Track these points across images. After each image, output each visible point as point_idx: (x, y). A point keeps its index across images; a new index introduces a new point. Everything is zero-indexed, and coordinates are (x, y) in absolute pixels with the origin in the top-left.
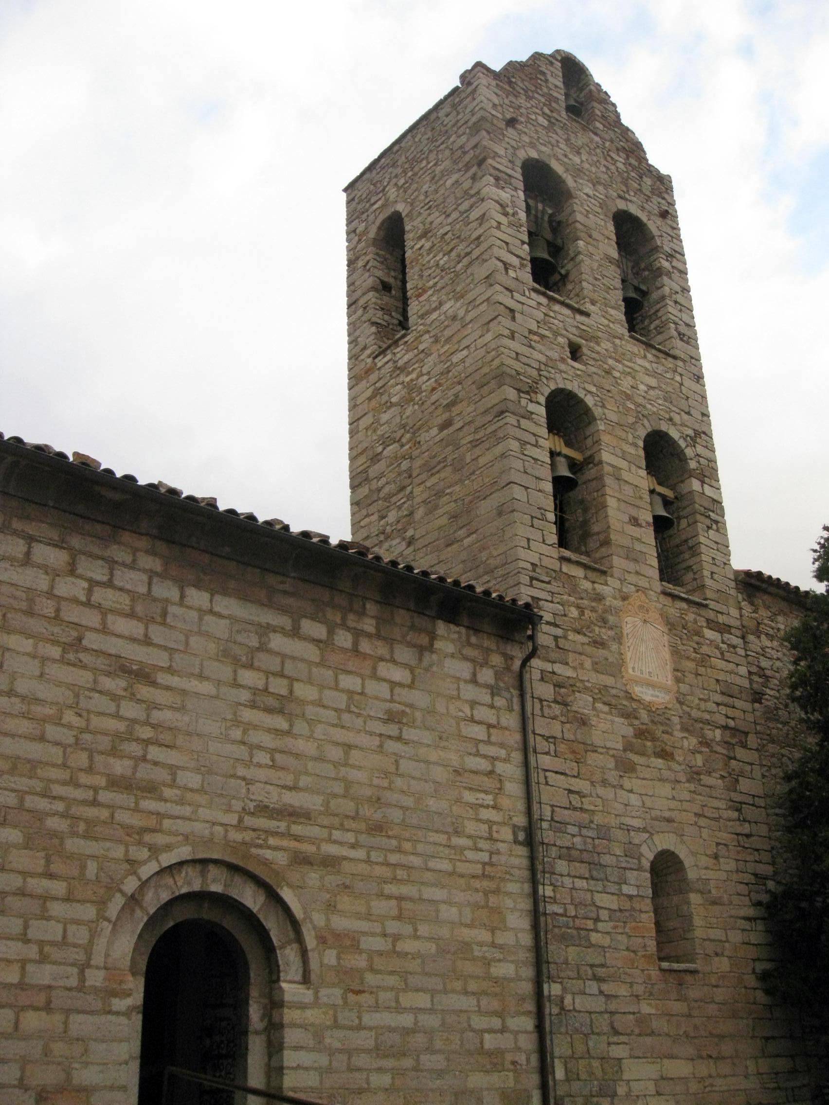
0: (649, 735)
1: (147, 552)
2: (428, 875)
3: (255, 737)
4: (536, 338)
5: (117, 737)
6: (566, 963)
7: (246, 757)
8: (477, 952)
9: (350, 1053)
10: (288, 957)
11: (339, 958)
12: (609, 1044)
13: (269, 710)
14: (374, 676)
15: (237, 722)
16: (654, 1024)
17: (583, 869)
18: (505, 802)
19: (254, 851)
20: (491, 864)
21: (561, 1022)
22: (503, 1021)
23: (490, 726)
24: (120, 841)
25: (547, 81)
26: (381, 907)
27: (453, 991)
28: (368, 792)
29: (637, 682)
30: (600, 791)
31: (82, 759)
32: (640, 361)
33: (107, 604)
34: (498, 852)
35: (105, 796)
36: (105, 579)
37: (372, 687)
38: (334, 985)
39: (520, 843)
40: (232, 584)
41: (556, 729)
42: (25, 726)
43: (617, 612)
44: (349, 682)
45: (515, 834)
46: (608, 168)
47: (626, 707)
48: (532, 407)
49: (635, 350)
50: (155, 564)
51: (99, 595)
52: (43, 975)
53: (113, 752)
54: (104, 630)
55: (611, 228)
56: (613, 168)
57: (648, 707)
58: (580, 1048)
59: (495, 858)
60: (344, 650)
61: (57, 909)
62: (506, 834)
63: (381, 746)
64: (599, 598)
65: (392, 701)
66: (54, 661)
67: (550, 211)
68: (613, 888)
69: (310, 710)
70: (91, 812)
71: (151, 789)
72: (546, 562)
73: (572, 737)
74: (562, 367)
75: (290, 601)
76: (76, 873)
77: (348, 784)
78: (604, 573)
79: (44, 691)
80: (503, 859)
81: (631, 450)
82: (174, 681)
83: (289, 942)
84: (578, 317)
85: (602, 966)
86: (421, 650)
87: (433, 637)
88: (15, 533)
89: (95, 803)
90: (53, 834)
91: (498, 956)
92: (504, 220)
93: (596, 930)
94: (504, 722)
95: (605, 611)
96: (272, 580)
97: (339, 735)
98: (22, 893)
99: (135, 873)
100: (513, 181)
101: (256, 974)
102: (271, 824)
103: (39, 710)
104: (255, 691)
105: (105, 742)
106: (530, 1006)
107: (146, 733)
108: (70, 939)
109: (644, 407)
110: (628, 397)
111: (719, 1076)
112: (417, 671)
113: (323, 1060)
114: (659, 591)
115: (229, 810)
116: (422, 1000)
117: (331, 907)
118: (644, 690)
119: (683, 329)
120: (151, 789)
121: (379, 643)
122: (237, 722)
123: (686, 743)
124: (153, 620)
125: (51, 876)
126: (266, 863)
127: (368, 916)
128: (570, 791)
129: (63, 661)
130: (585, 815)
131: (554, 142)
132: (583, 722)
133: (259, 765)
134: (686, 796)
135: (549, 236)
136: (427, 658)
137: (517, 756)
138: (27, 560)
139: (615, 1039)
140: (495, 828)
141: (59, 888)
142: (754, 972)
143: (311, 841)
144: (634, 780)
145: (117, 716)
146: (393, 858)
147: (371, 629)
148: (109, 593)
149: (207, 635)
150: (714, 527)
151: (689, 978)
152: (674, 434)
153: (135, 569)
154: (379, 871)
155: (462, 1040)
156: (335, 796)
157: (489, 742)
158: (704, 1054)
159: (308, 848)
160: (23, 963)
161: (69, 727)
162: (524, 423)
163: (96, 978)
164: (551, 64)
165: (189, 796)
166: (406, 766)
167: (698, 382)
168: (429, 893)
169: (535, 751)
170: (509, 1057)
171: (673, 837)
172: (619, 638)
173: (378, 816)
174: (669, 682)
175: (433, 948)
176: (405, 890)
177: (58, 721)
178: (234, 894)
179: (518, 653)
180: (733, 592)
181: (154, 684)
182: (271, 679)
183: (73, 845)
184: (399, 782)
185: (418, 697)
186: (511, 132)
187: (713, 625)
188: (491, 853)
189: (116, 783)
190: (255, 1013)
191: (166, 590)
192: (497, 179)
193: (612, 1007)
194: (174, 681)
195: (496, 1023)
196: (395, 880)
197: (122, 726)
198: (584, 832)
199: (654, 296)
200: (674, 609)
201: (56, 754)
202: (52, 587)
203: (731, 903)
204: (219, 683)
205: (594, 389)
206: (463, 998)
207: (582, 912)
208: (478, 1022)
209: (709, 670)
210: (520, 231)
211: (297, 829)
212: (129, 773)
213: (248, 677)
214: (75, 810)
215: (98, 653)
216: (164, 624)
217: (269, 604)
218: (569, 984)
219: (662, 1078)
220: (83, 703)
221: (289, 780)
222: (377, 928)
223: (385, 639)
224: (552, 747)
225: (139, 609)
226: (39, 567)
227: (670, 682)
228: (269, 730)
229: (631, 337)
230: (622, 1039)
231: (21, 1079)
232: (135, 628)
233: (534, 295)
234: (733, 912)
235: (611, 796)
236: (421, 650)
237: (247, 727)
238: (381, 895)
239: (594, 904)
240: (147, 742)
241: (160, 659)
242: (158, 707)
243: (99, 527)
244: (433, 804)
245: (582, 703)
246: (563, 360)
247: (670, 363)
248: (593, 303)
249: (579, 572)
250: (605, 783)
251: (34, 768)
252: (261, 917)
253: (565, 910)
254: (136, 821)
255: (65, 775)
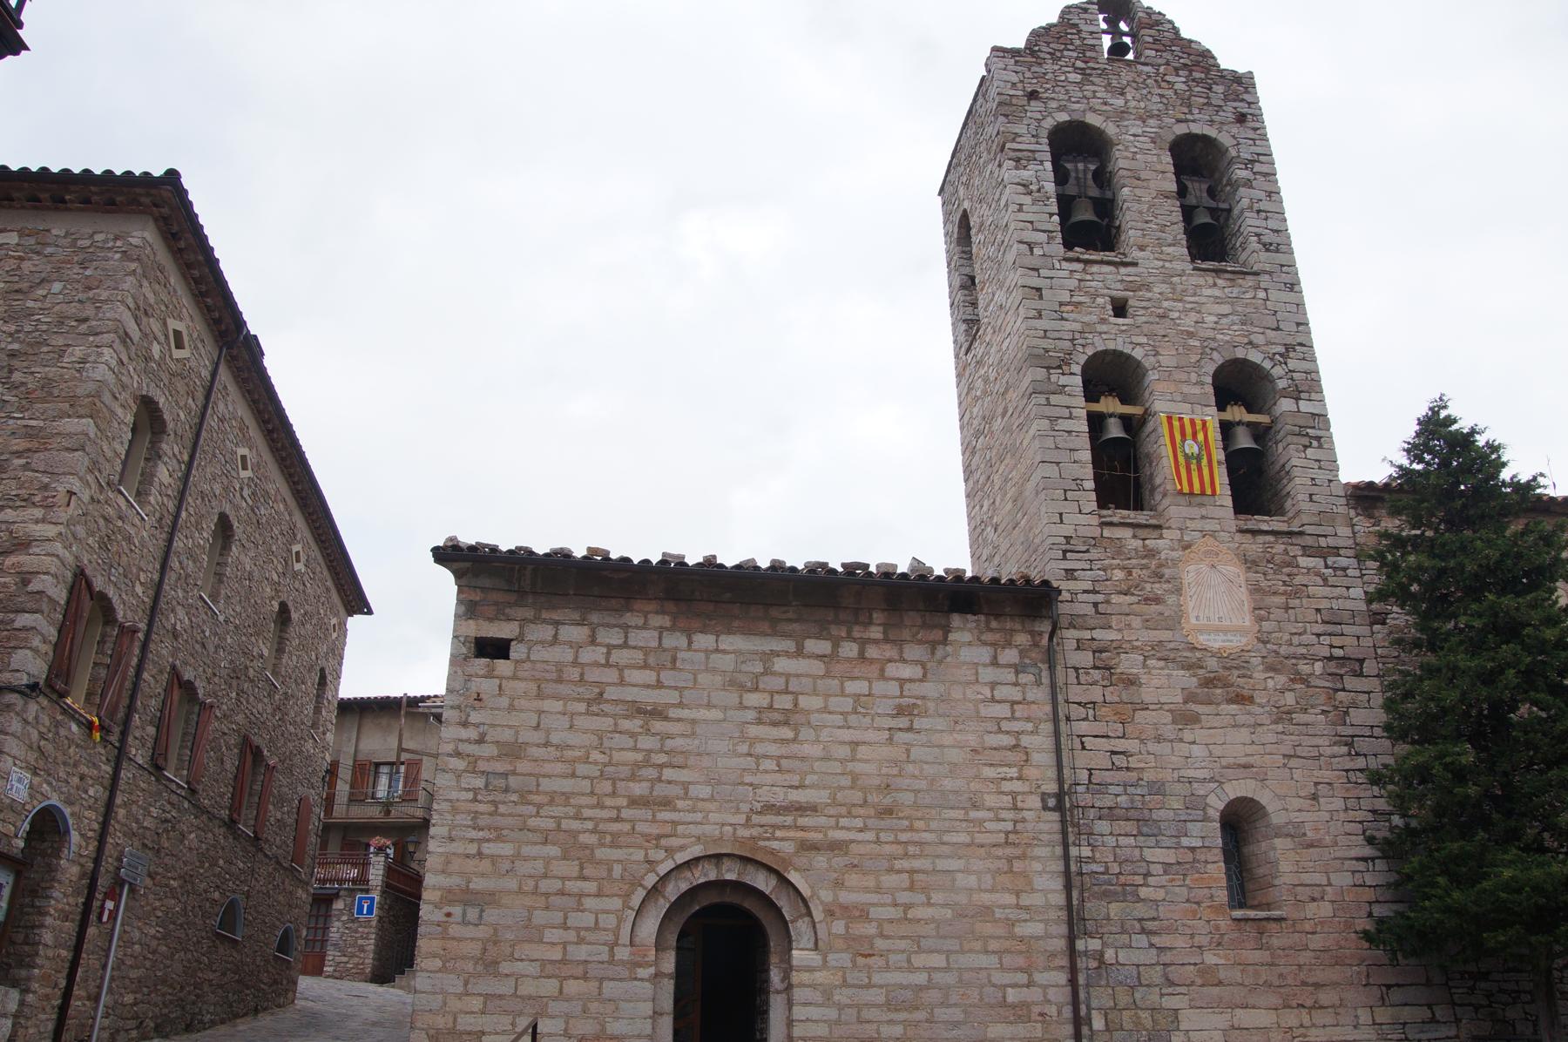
0: (1219, 682)
1: (657, 613)
2: (945, 848)
3: (759, 749)
4: (1069, 308)
5: (637, 765)
6: (1108, 919)
7: (754, 766)
8: (999, 914)
9: (859, 1008)
10: (800, 929)
11: (847, 928)
12: (1162, 995)
13: (775, 724)
14: (882, 676)
15: (743, 738)
16: (1222, 975)
17: (1130, 827)
18: (1032, 772)
19: (761, 843)
20: (1015, 832)
21: (1100, 975)
22: (1030, 975)
23: (1013, 703)
24: (641, 847)
25: (1080, 31)
26: (889, 880)
27: (971, 951)
28: (877, 781)
29: (1200, 631)
30: (1152, 747)
31: (607, 786)
32: (1209, 292)
33: (622, 662)
34: (1024, 820)
35: (625, 814)
36: (620, 642)
37: (879, 687)
38: (842, 951)
39: (1050, 809)
40: (736, 624)
41: (1096, 694)
42: (559, 768)
43: (1175, 563)
44: (852, 687)
45: (1043, 800)
46: (1162, 96)
47: (1189, 659)
48: (1063, 380)
49: (1201, 281)
50: (666, 621)
51: (616, 656)
52: (581, 953)
53: (633, 778)
54: (622, 682)
55: (1168, 158)
56: (1170, 92)
57: (1217, 654)
58: (1124, 999)
59: (1019, 826)
60: (849, 660)
61: (589, 903)
62: (1035, 802)
63: (891, 739)
64: (1151, 553)
65: (902, 696)
66: (581, 714)
67: (1092, 167)
68: (1167, 842)
69: (814, 718)
70: (615, 827)
71: (667, 803)
72: (1083, 531)
73: (1117, 699)
74: (1104, 328)
75: (796, 626)
76: (605, 874)
77: (855, 778)
78: (1159, 527)
79: (572, 738)
80: (1029, 826)
81: (1196, 390)
82: (685, 713)
83: (801, 916)
84: (1123, 270)
85: (1154, 919)
86: (933, 645)
87: (947, 630)
88: (544, 621)
89: (618, 819)
90: (586, 847)
91: (1026, 916)
92: (1027, 200)
93: (1146, 885)
94: (1030, 696)
95: (1160, 566)
96: (774, 612)
97: (847, 735)
98: (562, 893)
99: (654, 871)
100: (1037, 155)
101: (774, 943)
102: (779, 820)
103: (569, 754)
104: (760, 710)
105: (625, 771)
106: (1065, 962)
107: (662, 759)
108: (601, 925)
109: (1214, 339)
110: (1191, 335)
111: (1314, 1025)
112: (929, 665)
113: (833, 1014)
114: (1234, 529)
115: (738, 811)
116: (938, 960)
117: (838, 884)
118: (1212, 636)
119: (1268, 237)
120: (667, 803)
121: (888, 646)
122: (743, 738)
123: (1270, 683)
124: (663, 667)
125: (585, 879)
126: (773, 852)
127: (878, 889)
128: (1113, 753)
129: (588, 713)
130: (1134, 774)
131: (1089, 94)
132: (1131, 682)
133: (766, 772)
134: (1271, 738)
135: (1094, 192)
136: (940, 651)
137: (1047, 727)
138: (555, 641)
139: (1170, 990)
140: (1019, 798)
141: (591, 887)
142: (1370, 915)
143: (816, 829)
144: (1197, 731)
145: (635, 749)
146: (904, 837)
147: (880, 636)
148: (625, 653)
149: (714, 671)
150: (1315, 443)
151: (1273, 926)
152: (1255, 357)
153: (647, 630)
154: (888, 849)
155: (981, 994)
156: (841, 788)
157: (1013, 718)
158: (1294, 1004)
159: (815, 836)
160: (565, 945)
161: (596, 763)
162: (1054, 399)
163: (623, 953)
164: (1086, 11)
165: (700, 805)
166: (916, 753)
167: (1292, 290)
168: (942, 864)
169: (1068, 719)
170: (1036, 1009)
171: (1252, 784)
172: (1178, 591)
173: (888, 801)
174: (1247, 623)
175: (949, 913)
176: (917, 864)
177: (586, 760)
178: (747, 880)
179: (1045, 627)
180: (1342, 510)
181: (666, 718)
182: (776, 697)
183: (600, 853)
184: (910, 768)
185: (929, 689)
186: (1035, 105)
187: (1308, 551)
188: (1015, 822)
189: (634, 802)
190: (775, 977)
191: (675, 640)
192: (1018, 160)
193: (1166, 958)
194: (685, 713)
195: (1022, 978)
196: (906, 855)
197: (640, 757)
198: (1130, 790)
199: (1236, 212)
200: (1254, 547)
201: (585, 785)
202: (576, 657)
203: (1336, 844)
204: (725, 709)
205: (1145, 340)
206: (983, 957)
207: (1128, 868)
208: (998, 978)
209: (1305, 601)
210: (1117, 185)
211: (802, 821)
212: (646, 792)
213: (753, 699)
214: (601, 827)
215: (616, 702)
216: (674, 668)
217: (775, 633)
218: (1110, 939)
219: (1233, 1027)
220: (606, 743)
221: (795, 780)
222: (888, 899)
223: (894, 642)
224: (1091, 712)
225: (651, 661)
226: (565, 643)
227: (1247, 621)
228: (775, 741)
229: (1195, 269)
230: (1179, 990)
231: (566, 1030)
232: (649, 676)
233: (1065, 265)
234: (1338, 854)
235: (1169, 751)
236: (933, 645)
237: (754, 741)
238: (891, 870)
239: (1143, 859)
240: (661, 766)
241: (672, 697)
242: (670, 737)
243: (613, 601)
244: (948, 784)
245: (1129, 664)
246: (1103, 321)
247: (1250, 281)
248: (1142, 248)
249: (1126, 533)
250: (1159, 739)
251: (568, 798)
252: (773, 897)
253: (1107, 868)
254: (654, 830)
255: (594, 800)
